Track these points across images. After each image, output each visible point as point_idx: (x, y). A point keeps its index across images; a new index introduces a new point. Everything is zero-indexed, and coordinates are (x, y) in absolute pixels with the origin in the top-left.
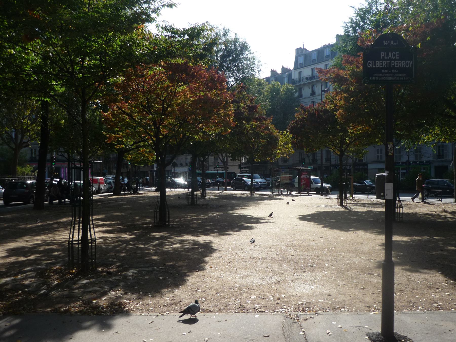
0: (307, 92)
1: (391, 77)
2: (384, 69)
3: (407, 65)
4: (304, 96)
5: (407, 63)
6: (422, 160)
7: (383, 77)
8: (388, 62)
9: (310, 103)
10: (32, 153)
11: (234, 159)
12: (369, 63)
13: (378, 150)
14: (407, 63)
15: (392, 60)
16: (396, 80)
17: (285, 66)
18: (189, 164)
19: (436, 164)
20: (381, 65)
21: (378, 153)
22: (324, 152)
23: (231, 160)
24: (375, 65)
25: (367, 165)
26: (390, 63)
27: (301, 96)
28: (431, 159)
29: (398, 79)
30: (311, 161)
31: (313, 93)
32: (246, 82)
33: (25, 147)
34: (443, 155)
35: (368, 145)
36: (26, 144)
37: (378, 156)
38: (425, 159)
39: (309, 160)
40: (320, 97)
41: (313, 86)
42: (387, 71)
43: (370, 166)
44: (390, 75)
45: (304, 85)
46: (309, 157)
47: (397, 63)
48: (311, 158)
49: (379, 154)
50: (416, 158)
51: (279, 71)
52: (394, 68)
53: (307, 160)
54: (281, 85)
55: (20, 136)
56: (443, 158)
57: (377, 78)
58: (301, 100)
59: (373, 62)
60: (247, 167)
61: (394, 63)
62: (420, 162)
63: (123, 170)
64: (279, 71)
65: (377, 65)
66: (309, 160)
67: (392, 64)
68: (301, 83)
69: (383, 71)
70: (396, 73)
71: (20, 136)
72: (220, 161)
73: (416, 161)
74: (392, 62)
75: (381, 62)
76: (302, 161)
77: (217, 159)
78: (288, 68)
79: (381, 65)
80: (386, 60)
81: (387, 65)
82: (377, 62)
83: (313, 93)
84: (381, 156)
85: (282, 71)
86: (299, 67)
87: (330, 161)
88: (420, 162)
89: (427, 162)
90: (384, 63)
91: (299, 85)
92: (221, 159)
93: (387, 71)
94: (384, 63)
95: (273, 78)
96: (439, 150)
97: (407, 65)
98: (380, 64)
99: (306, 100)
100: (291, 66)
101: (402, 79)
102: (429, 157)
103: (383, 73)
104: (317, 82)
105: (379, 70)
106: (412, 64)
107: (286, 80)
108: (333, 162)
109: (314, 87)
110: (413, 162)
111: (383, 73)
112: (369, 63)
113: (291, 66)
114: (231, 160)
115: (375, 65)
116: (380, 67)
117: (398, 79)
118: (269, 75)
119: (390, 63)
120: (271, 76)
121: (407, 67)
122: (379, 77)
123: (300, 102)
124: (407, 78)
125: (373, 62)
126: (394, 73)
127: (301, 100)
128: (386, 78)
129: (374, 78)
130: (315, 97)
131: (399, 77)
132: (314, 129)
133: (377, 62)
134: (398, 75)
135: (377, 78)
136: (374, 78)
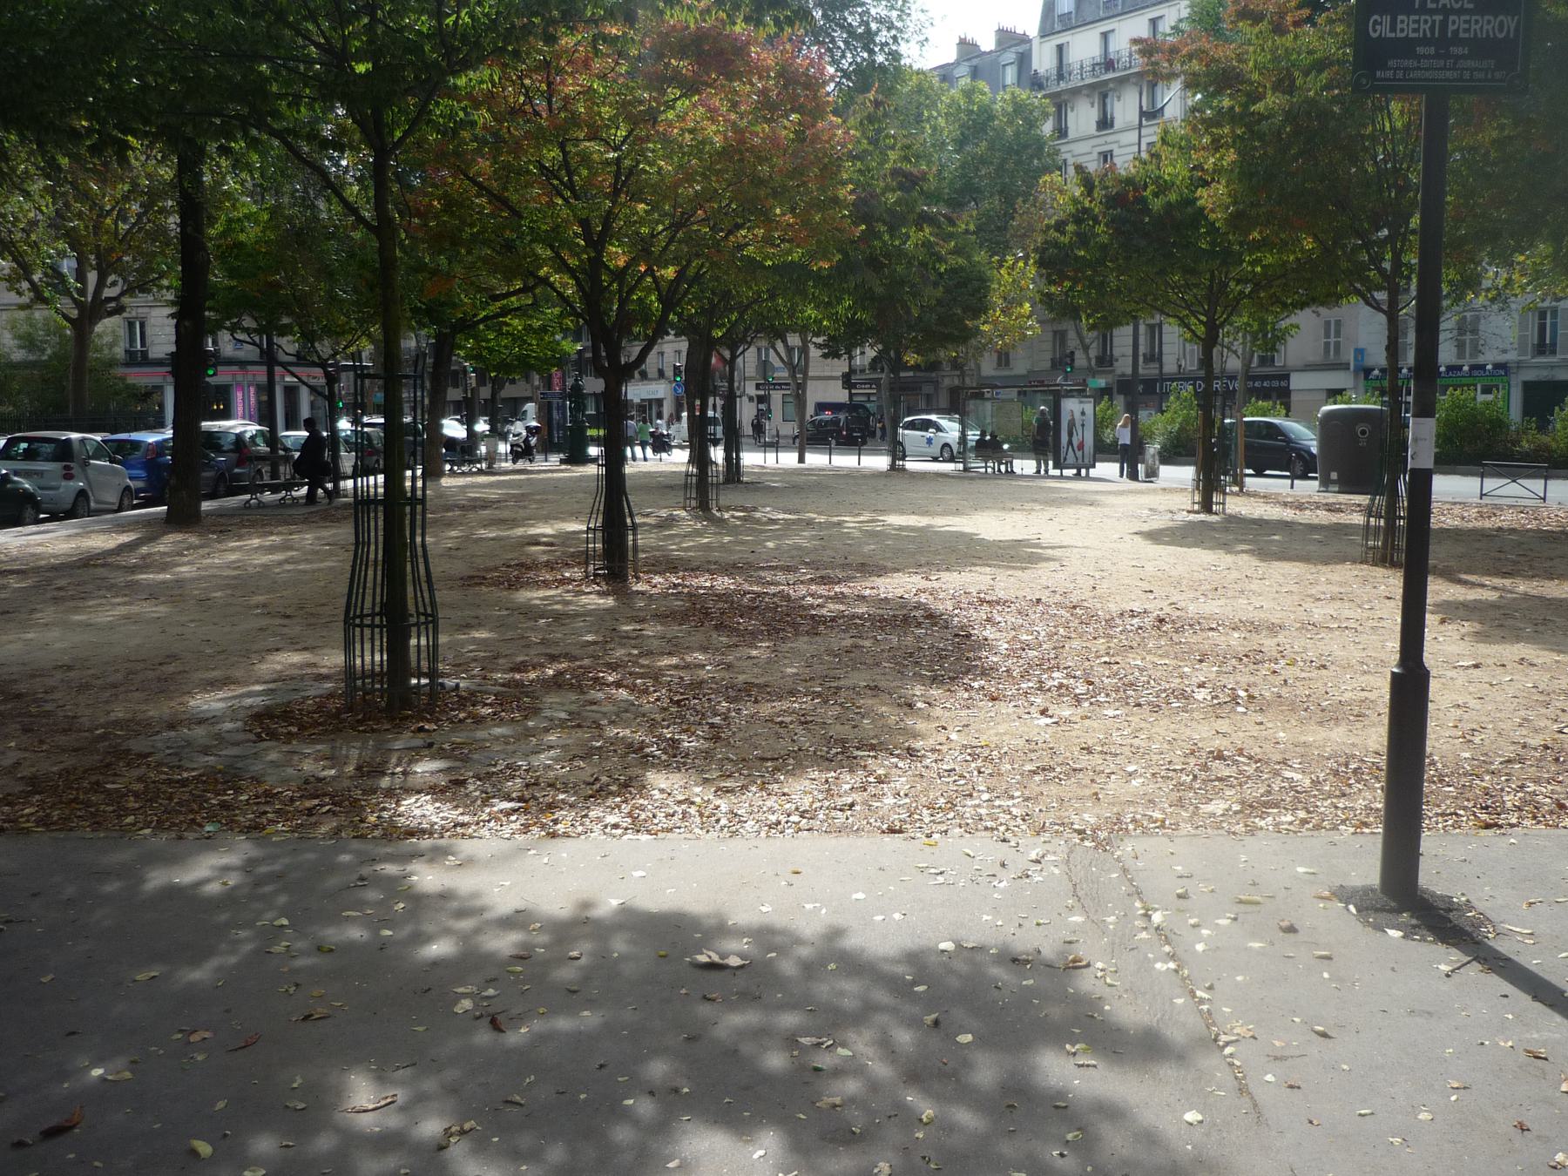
0: (1083, 118)
1: (1444, 68)
2: (1424, 41)
3: (1501, 30)
4: (1072, 134)
5: (1501, 23)
6: (1481, 360)
7: (1419, 68)
8: (1438, 18)
9: (1095, 155)
10: (132, 340)
11: (831, 353)
12: (1376, 22)
13: (1328, 323)
14: (1501, 23)
15: (1453, 11)
16: (1461, 79)
17: (1008, 25)
18: (669, 373)
19: (1530, 376)
20: (1415, 30)
21: (1327, 335)
22: (1142, 329)
23: (825, 356)
24: (1393, 29)
25: (1287, 377)
26: (1444, 24)
27: (1061, 132)
28: (1511, 356)
29: (1467, 75)
30: (1093, 362)
31: (1105, 123)
32: (879, 79)
33: (111, 314)
34: (1554, 344)
35: (1302, 305)
36: (113, 304)
37: (1327, 345)
38: (1489, 358)
39: (1089, 359)
40: (1132, 137)
41: (1104, 96)
42: (1432, 50)
43: (1297, 382)
44: (1442, 63)
45: (1076, 92)
46: (1086, 348)
47: (1469, 22)
48: (1093, 353)
49: (1332, 340)
50: (1461, 355)
51: (987, 44)
52: (1456, 40)
53: (1080, 360)
54: (994, 91)
55: (92, 277)
56: (1553, 352)
57: (1400, 74)
58: (1063, 149)
59: (1387, 19)
60: (870, 382)
61: (1456, 23)
62: (1473, 368)
63: (454, 394)
64: (987, 44)
65: (1402, 30)
66: (1089, 359)
67: (1451, 28)
68: (1063, 86)
69: (1420, 50)
70: (1463, 57)
71: (92, 277)
72: (777, 363)
73: (1460, 362)
74: (1451, 18)
75: (1413, 17)
76: (1063, 361)
77: (767, 355)
78: (1020, 31)
79: (1415, 30)
80: (1432, 12)
81: (1432, 29)
82: (1400, 18)
83: (1105, 123)
84: (1337, 345)
85: (999, 42)
86: (1057, 27)
87: (1160, 360)
88: (1473, 367)
89: (1497, 366)
90: (1426, 22)
91: (1058, 94)
92: (783, 355)
93: (1432, 50)
94: (1426, 22)
95: (963, 70)
96: (1542, 328)
97: (1501, 30)
98: (1412, 26)
99: (1080, 148)
100: (1028, 22)
101: (1481, 75)
102: (1505, 351)
103: (1419, 58)
104: (1122, 81)
105: (1406, 47)
106: (1517, 30)
107: (1010, 75)
108: (1170, 366)
109: (1108, 101)
110: (1450, 368)
111: (1419, 58)
112: (1376, 22)
113: (1028, 22)
114: (825, 356)
115: (1393, 29)
116: (1412, 35)
117: (1467, 75)
118: (949, 55)
119: (1444, 24)
120: (957, 63)
121: (1501, 36)
122: (1405, 69)
123: (1057, 152)
124: (1498, 75)
125: (1387, 19)
126: (1458, 57)
127: (1063, 149)
128: (1427, 74)
129: (1389, 74)
130: (1110, 138)
131: (1472, 70)
132: (1133, 248)
133: (1400, 18)
134: (1470, 63)
135: (1400, 74)
136: (1389, 74)
